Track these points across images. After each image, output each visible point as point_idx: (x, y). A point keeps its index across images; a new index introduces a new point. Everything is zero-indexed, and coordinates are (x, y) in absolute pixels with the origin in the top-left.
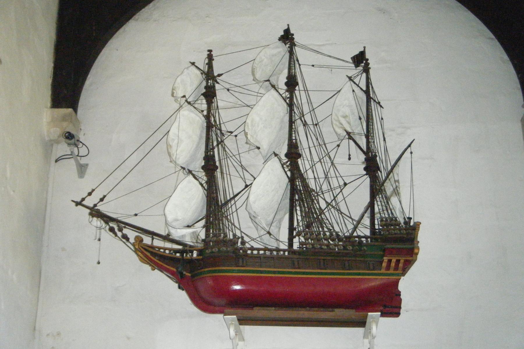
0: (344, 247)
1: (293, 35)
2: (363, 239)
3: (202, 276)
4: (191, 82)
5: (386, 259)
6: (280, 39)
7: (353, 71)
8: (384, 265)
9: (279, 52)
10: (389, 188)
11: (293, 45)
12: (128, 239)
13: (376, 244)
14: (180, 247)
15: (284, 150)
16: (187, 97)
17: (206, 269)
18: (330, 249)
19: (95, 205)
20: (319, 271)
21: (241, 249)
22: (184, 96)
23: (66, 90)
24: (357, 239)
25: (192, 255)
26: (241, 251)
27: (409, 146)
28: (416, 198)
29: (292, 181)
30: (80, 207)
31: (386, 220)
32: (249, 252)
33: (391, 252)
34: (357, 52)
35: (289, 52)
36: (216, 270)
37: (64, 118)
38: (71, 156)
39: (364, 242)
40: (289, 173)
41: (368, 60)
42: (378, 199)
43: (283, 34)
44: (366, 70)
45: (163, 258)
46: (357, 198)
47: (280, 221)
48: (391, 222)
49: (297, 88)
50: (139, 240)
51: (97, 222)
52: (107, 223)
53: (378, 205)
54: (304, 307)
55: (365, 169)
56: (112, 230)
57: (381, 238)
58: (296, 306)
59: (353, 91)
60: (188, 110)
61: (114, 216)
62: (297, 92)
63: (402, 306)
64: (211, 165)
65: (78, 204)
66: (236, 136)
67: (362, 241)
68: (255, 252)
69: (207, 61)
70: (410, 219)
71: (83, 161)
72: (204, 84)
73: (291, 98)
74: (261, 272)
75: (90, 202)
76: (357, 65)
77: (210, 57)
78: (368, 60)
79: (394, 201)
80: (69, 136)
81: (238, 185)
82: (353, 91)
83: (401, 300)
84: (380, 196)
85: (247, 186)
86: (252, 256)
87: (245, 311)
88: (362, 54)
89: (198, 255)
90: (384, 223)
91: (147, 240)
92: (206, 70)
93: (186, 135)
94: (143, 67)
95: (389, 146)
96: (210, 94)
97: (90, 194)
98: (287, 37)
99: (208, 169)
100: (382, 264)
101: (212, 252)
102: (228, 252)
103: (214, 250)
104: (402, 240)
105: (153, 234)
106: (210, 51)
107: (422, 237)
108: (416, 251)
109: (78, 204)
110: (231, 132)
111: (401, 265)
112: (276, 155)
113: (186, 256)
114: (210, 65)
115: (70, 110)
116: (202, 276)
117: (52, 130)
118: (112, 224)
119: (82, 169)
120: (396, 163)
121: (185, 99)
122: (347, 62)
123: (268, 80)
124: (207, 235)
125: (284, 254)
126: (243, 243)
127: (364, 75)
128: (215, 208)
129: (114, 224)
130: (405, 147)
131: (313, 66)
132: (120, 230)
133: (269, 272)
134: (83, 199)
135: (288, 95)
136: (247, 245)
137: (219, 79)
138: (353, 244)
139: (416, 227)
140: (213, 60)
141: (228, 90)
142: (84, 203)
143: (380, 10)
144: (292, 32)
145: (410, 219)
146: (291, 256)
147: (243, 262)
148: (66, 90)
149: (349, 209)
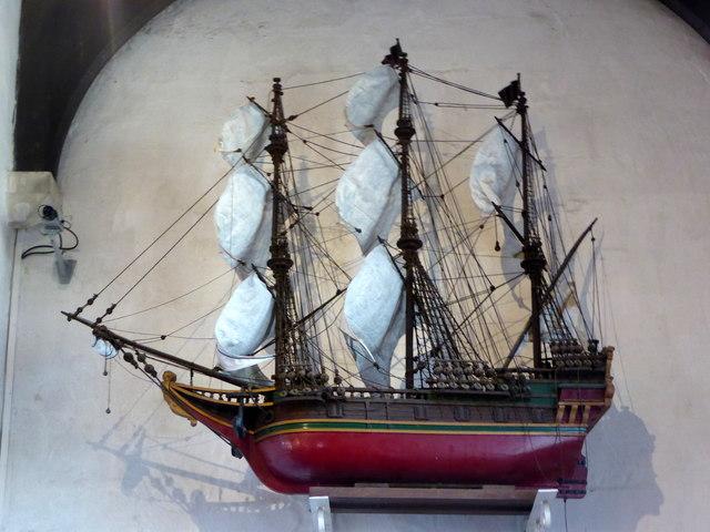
0: (496, 386)
1: (405, 55)
2: (526, 375)
3: (273, 434)
4: (243, 128)
5: (562, 405)
6: (383, 63)
7: (503, 112)
8: (560, 415)
9: (385, 82)
10: (561, 292)
11: (405, 69)
12: (154, 374)
13: (545, 381)
14: (238, 389)
15: (394, 235)
16: (243, 151)
17: (279, 423)
18: (475, 389)
19: (99, 320)
20: (457, 424)
21: (335, 389)
22: (239, 151)
23: (42, 142)
24: (515, 374)
25: (257, 400)
26: (335, 394)
27: (590, 229)
28: (612, 307)
29: (407, 283)
30: (73, 321)
31: (561, 344)
32: (348, 394)
33: (570, 393)
34: (507, 84)
35: (400, 82)
36: (318, 427)
37: (38, 187)
38: (51, 250)
39: (528, 378)
40: (404, 272)
41: (524, 93)
42: (546, 311)
43: (389, 53)
44: (522, 110)
45: (208, 406)
46: (510, 307)
47: (394, 346)
48: (566, 347)
49: (413, 138)
50: (171, 378)
51: (104, 346)
52: (118, 347)
53: (546, 321)
54: (434, 483)
55: (523, 265)
56: (128, 358)
57: (553, 373)
58: (423, 482)
59: (505, 141)
60: (246, 172)
61: (129, 337)
62: (413, 145)
63: (589, 479)
64: (283, 259)
65: (71, 317)
66: (317, 214)
67: (524, 377)
68: (356, 394)
69: (273, 97)
70: (596, 342)
71: (68, 255)
72: (269, 131)
73: (405, 154)
74: (366, 426)
75: (90, 315)
76: (508, 105)
77: (278, 90)
78: (524, 93)
79: (571, 315)
80: (49, 213)
81: (325, 291)
82: (505, 141)
83: (586, 469)
84: (549, 306)
85: (339, 292)
86: (353, 401)
87: (359, 496)
88: (515, 85)
89: (266, 401)
90: (556, 348)
91: (184, 377)
92: (272, 110)
93: (239, 208)
94: (173, 107)
95: (562, 230)
96: (278, 149)
97: (90, 302)
98: (396, 57)
99: (277, 266)
100: (556, 414)
101: (289, 395)
102: (315, 395)
103: (292, 392)
104: (585, 376)
105: (193, 368)
106: (277, 80)
107: (617, 370)
108: (609, 390)
109: (71, 317)
110: (310, 209)
111: (586, 416)
112: (381, 241)
113: (247, 401)
114: (277, 101)
115: (46, 174)
116: (273, 434)
117: (18, 206)
118: (128, 350)
119: (66, 271)
120: (574, 250)
121: (240, 155)
122: (493, 97)
123: (371, 126)
124: (279, 369)
125: (212, 397)
126: (338, 380)
127: (519, 117)
128: (284, 326)
129: (135, 353)
130: (584, 230)
131: (436, 104)
132: (142, 359)
133: (378, 426)
134: (80, 310)
135: (399, 149)
136: (345, 384)
137: (289, 125)
138: (508, 381)
139: (607, 355)
140: (282, 94)
141: (305, 142)
142: (81, 315)
143: (537, 16)
144: (404, 50)
145: (596, 342)
146: (411, 401)
147: (338, 410)
148: (42, 142)
149: (495, 324)
